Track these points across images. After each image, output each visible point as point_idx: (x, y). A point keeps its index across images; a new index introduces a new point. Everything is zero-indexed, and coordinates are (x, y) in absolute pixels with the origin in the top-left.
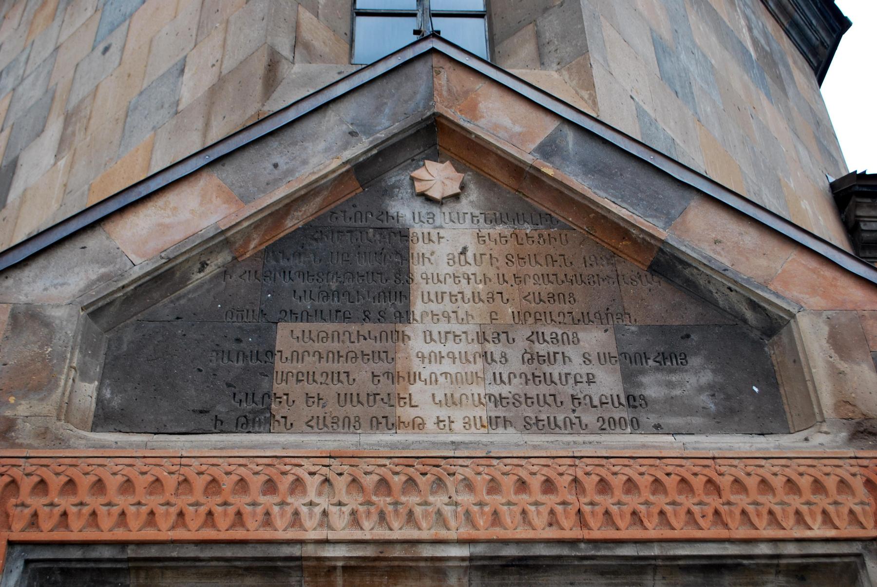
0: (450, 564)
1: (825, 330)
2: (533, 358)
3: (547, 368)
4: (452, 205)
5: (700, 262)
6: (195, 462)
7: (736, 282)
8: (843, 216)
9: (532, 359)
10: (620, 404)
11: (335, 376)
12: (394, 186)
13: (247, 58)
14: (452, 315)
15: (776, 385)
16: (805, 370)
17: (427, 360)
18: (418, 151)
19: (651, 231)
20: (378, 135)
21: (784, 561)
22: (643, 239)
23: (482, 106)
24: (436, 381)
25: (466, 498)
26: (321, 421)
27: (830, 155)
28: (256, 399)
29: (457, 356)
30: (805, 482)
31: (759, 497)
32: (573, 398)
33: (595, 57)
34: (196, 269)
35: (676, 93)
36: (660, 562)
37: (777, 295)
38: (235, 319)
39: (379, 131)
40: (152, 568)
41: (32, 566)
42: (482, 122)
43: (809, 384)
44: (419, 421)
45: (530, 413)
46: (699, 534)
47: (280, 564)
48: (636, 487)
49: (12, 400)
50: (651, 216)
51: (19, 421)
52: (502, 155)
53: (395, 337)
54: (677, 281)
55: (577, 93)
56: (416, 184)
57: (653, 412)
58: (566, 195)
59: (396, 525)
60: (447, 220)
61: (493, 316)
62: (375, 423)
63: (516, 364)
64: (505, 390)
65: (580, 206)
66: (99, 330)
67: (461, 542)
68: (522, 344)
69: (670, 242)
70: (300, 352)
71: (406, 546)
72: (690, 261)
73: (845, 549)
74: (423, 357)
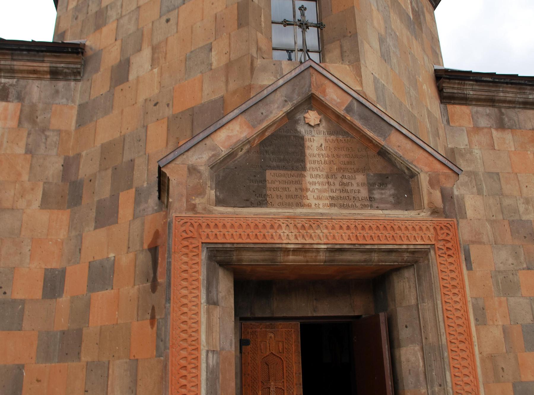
0: (321, 250)
1: (428, 178)
2: (343, 184)
3: (347, 188)
4: (317, 127)
5: (393, 154)
6: (250, 219)
7: (403, 161)
8: (438, 84)
9: (342, 184)
10: (367, 200)
11: (285, 189)
12: (299, 120)
13: (241, 57)
14: (318, 168)
15: (412, 195)
16: (421, 191)
17: (311, 184)
18: (305, 106)
19: (379, 142)
20: (294, 102)
21: (409, 250)
22: (377, 144)
23: (327, 90)
24: (314, 191)
25: (325, 231)
26: (282, 204)
27: (436, 53)
28: (262, 196)
29: (320, 183)
30: (417, 228)
31: (405, 232)
32: (354, 197)
33: (362, 62)
34: (240, 151)
35: (385, 60)
36: (377, 250)
37: (415, 166)
38: (253, 169)
39: (294, 100)
40: (241, 250)
41: (208, 249)
42: (327, 97)
43: (421, 196)
44: (310, 204)
45: (341, 202)
46: (388, 243)
47: (276, 249)
48: (372, 228)
49: (194, 198)
50: (380, 136)
51: (197, 205)
52: (334, 111)
53: (302, 176)
54: (386, 158)
55: (355, 77)
56: (306, 119)
57: (376, 203)
58: (353, 127)
59: (307, 239)
60: (316, 134)
61: (330, 169)
62: (297, 205)
63: (338, 187)
64: (334, 195)
65: (358, 131)
66: (213, 172)
67: (324, 244)
68: (339, 179)
69: (385, 146)
70: (274, 180)
71: (310, 245)
72: (390, 153)
73: (426, 247)
74: (310, 183)
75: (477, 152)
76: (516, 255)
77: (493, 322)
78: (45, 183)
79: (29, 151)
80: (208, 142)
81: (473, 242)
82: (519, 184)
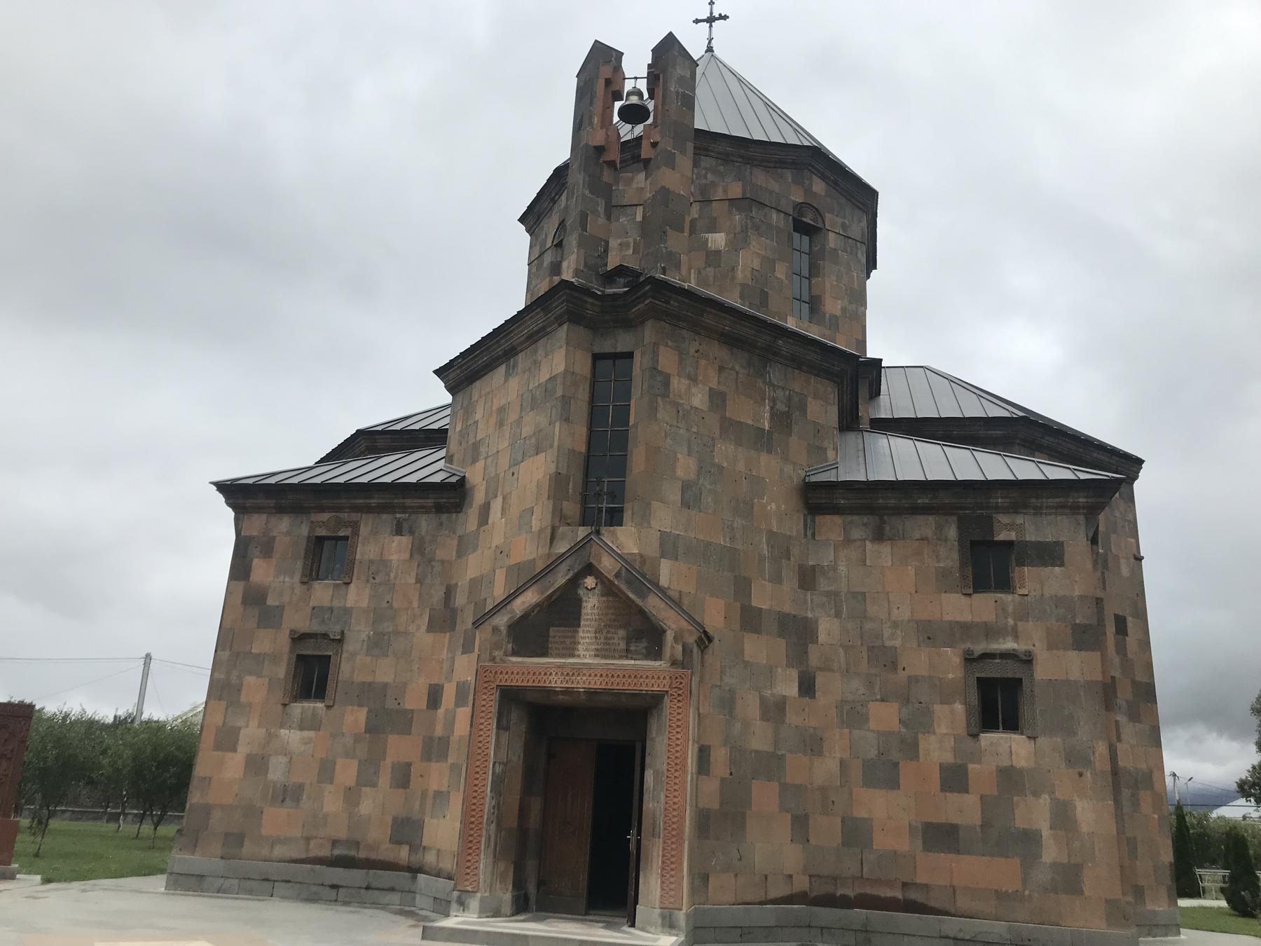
3: (609, 641)
63: (602, 640)
64: (599, 647)
75: (842, 568)
76: (870, 685)
77: (830, 754)
78: (430, 610)
79: (419, 581)
80: (508, 607)
81: (820, 669)
82: (889, 605)
